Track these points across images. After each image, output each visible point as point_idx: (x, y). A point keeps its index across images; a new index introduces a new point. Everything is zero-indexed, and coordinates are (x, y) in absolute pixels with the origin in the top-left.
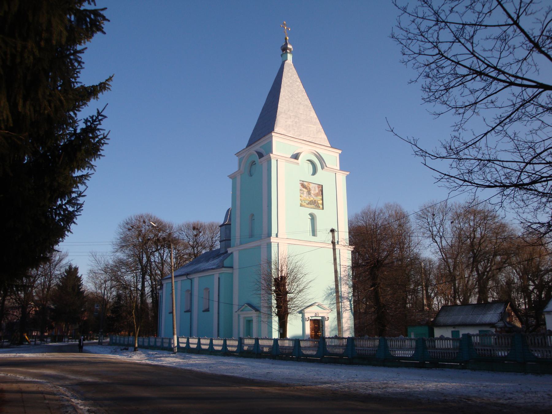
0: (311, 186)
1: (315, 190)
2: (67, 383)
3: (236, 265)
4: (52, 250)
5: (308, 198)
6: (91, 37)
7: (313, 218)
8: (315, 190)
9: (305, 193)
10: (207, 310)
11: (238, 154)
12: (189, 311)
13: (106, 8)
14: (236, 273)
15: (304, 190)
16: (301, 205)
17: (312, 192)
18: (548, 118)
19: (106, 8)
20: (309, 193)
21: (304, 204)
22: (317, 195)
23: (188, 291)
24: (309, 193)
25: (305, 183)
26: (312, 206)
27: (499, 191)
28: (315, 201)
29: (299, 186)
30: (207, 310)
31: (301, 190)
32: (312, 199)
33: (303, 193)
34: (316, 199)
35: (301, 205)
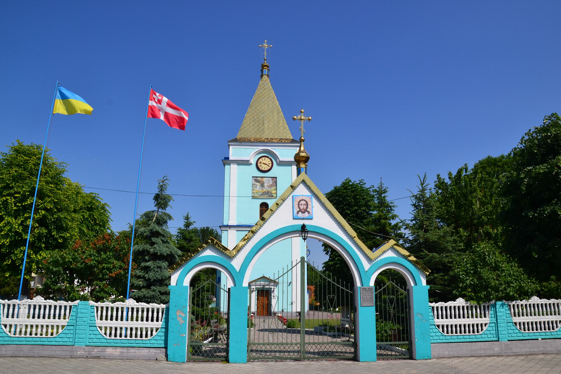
5: (261, 190)
17: (266, 185)
20: (262, 185)
21: (256, 195)
22: (271, 186)
24: (262, 185)
29: (251, 181)
31: (253, 185)
32: (265, 190)
33: (256, 187)
34: (269, 189)
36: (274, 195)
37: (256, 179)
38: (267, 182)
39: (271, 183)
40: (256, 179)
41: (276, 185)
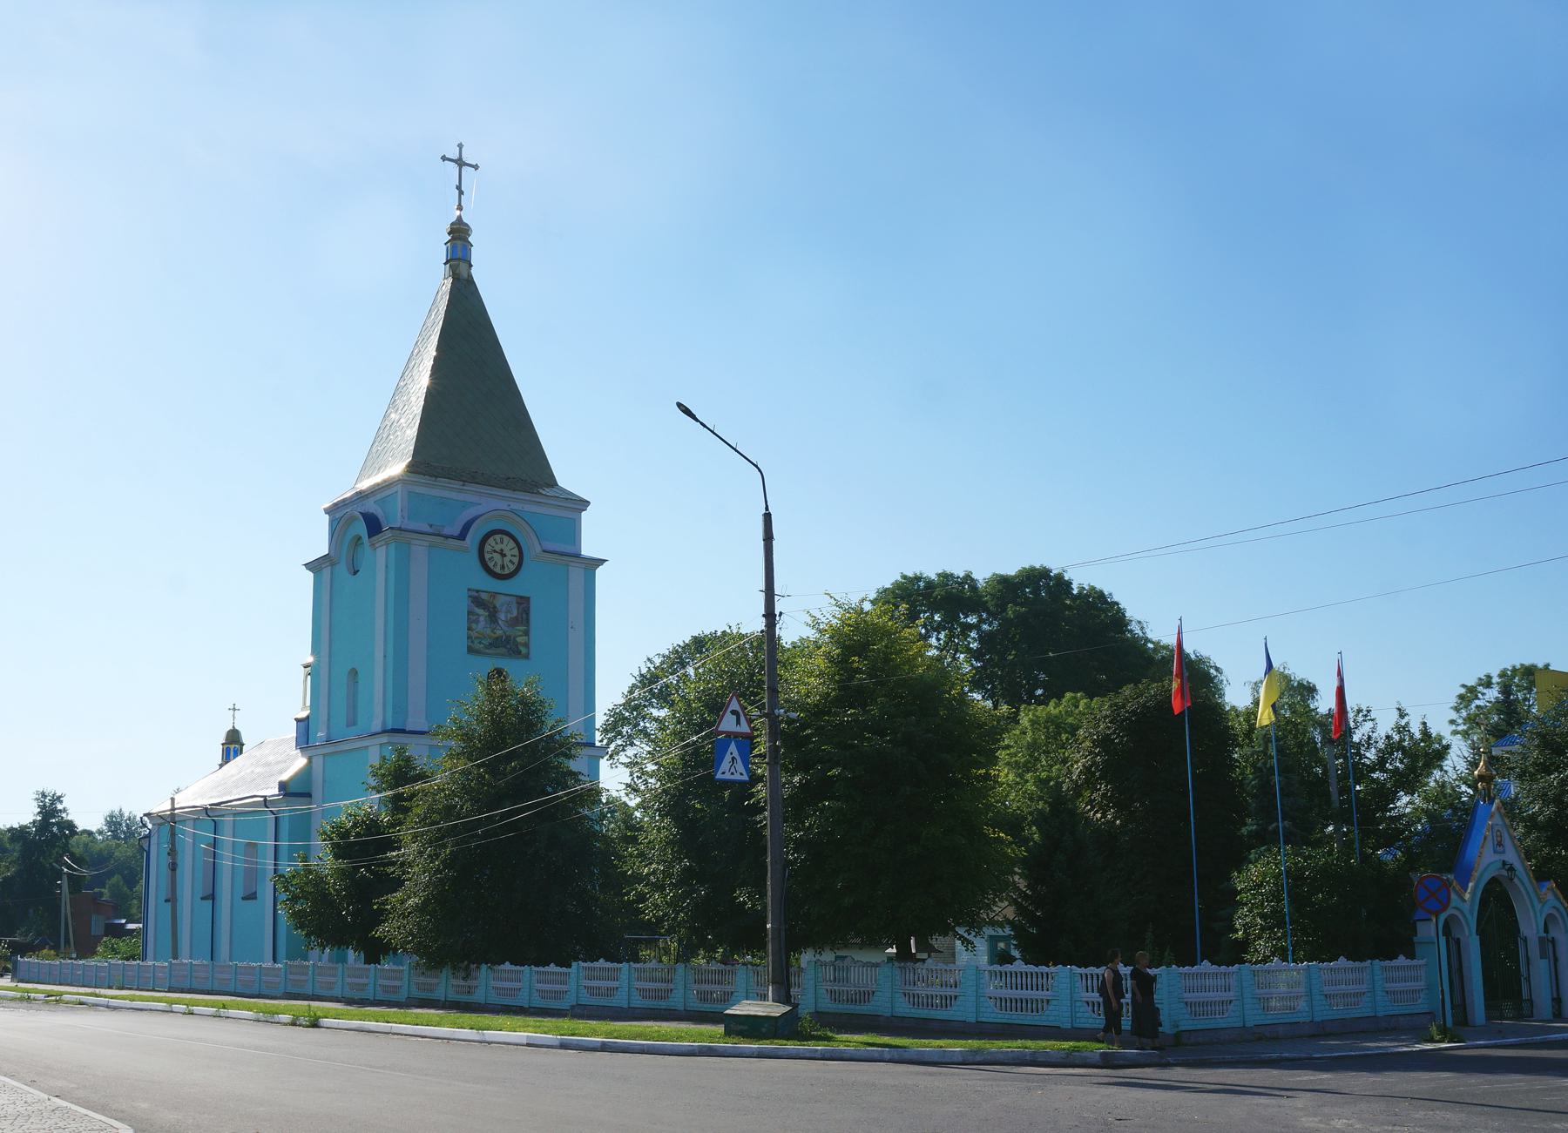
0: (499, 602)
5: (488, 631)
6: (1044, 573)
8: (508, 611)
10: (251, 897)
11: (328, 511)
12: (212, 897)
13: (679, 405)
15: (481, 611)
16: (471, 650)
17: (502, 616)
18: (2, 1113)
19: (679, 405)
20: (493, 617)
21: (477, 646)
24: (493, 617)
25: (484, 596)
26: (503, 650)
28: (508, 637)
29: (464, 604)
30: (251, 897)
31: (469, 613)
32: (499, 632)
33: (477, 622)
34: (509, 631)
35: (471, 650)
36: (523, 650)
37: (477, 600)
39: (515, 613)
40: (477, 600)
41: (528, 620)
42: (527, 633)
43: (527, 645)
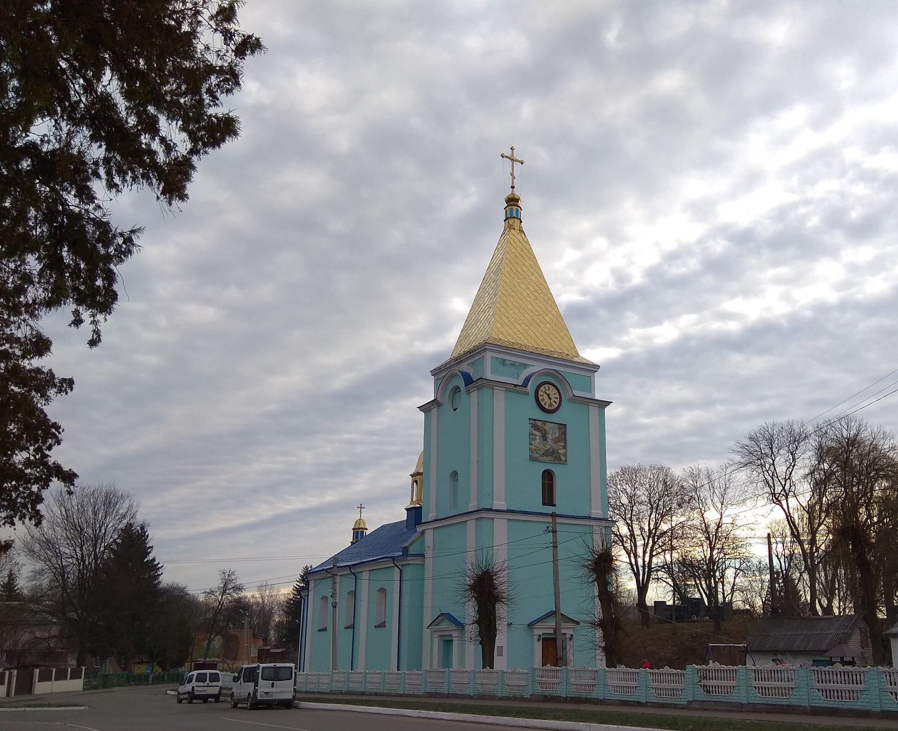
0: (548, 427)
1: (553, 433)
2: (272, 633)
3: (429, 554)
4: (207, 607)
7: (548, 476)
9: (537, 437)
14: (429, 561)
15: (537, 433)
16: (532, 458)
17: (550, 436)
20: (544, 437)
22: (557, 440)
23: (350, 593)
24: (544, 437)
25: (539, 423)
26: (550, 458)
27: (580, 574)
29: (527, 428)
30: (382, 625)
31: (530, 434)
33: (535, 439)
36: (563, 458)
38: (553, 433)
40: (535, 425)
42: (565, 447)
43: (565, 455)
